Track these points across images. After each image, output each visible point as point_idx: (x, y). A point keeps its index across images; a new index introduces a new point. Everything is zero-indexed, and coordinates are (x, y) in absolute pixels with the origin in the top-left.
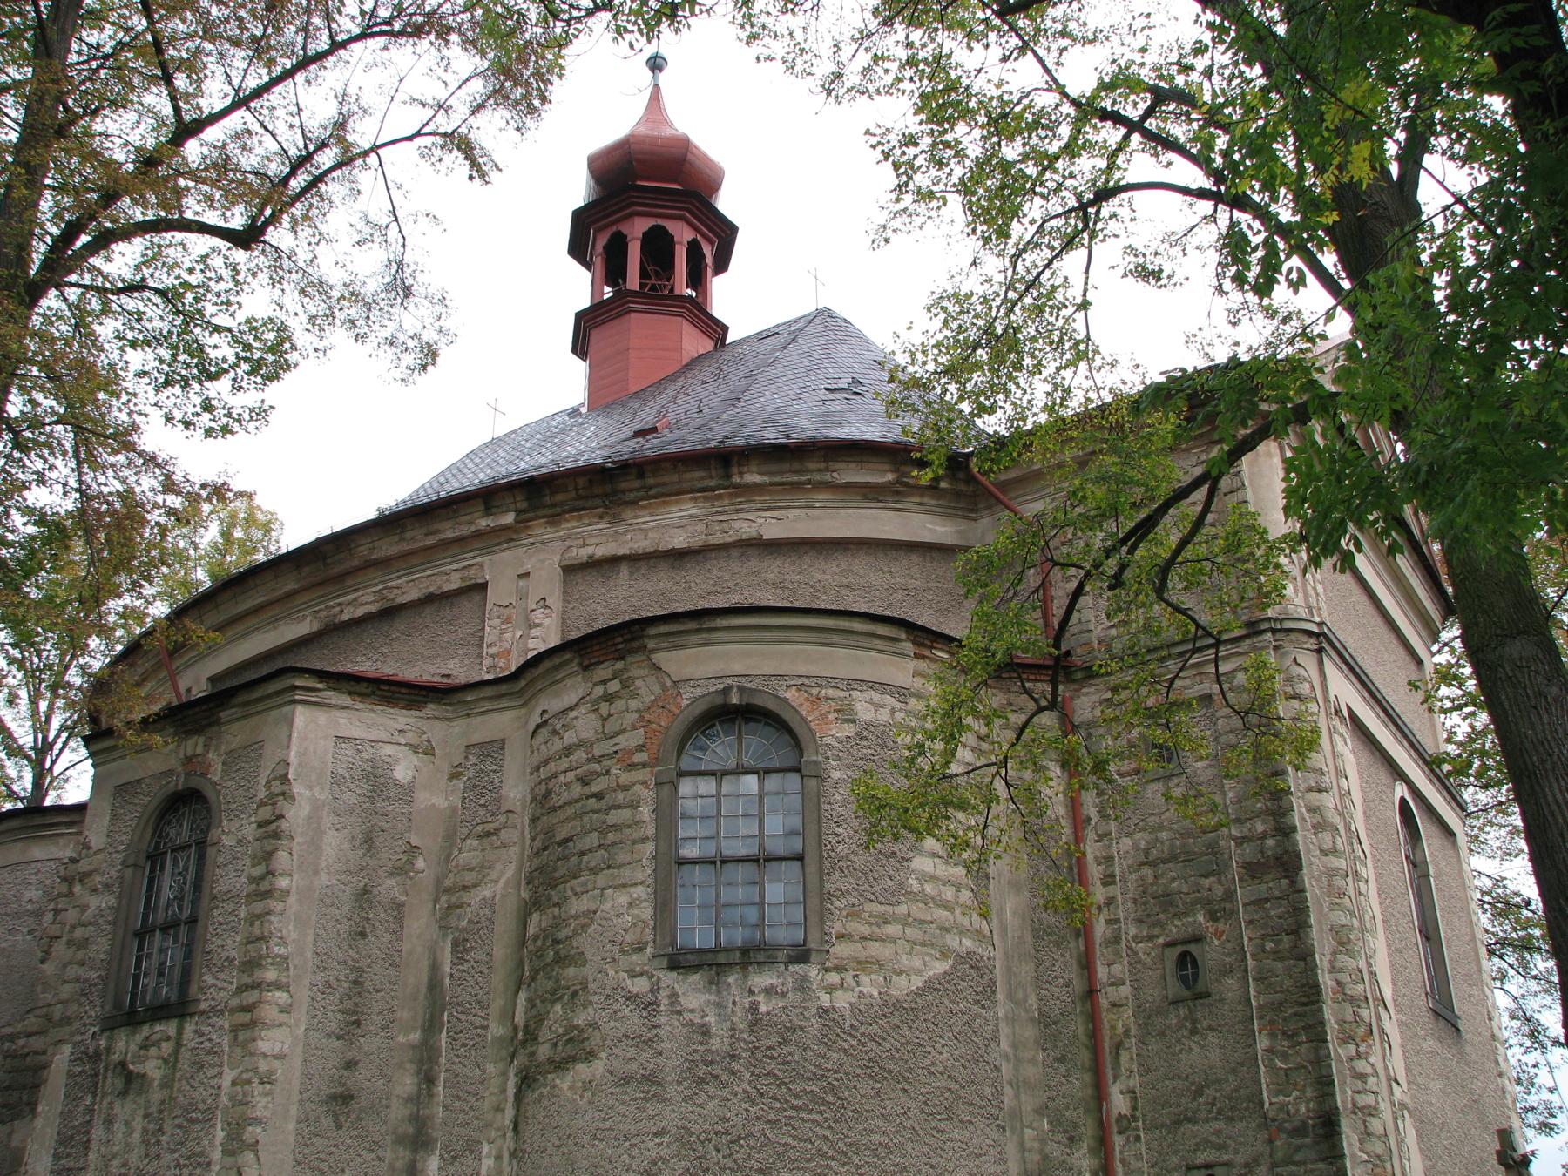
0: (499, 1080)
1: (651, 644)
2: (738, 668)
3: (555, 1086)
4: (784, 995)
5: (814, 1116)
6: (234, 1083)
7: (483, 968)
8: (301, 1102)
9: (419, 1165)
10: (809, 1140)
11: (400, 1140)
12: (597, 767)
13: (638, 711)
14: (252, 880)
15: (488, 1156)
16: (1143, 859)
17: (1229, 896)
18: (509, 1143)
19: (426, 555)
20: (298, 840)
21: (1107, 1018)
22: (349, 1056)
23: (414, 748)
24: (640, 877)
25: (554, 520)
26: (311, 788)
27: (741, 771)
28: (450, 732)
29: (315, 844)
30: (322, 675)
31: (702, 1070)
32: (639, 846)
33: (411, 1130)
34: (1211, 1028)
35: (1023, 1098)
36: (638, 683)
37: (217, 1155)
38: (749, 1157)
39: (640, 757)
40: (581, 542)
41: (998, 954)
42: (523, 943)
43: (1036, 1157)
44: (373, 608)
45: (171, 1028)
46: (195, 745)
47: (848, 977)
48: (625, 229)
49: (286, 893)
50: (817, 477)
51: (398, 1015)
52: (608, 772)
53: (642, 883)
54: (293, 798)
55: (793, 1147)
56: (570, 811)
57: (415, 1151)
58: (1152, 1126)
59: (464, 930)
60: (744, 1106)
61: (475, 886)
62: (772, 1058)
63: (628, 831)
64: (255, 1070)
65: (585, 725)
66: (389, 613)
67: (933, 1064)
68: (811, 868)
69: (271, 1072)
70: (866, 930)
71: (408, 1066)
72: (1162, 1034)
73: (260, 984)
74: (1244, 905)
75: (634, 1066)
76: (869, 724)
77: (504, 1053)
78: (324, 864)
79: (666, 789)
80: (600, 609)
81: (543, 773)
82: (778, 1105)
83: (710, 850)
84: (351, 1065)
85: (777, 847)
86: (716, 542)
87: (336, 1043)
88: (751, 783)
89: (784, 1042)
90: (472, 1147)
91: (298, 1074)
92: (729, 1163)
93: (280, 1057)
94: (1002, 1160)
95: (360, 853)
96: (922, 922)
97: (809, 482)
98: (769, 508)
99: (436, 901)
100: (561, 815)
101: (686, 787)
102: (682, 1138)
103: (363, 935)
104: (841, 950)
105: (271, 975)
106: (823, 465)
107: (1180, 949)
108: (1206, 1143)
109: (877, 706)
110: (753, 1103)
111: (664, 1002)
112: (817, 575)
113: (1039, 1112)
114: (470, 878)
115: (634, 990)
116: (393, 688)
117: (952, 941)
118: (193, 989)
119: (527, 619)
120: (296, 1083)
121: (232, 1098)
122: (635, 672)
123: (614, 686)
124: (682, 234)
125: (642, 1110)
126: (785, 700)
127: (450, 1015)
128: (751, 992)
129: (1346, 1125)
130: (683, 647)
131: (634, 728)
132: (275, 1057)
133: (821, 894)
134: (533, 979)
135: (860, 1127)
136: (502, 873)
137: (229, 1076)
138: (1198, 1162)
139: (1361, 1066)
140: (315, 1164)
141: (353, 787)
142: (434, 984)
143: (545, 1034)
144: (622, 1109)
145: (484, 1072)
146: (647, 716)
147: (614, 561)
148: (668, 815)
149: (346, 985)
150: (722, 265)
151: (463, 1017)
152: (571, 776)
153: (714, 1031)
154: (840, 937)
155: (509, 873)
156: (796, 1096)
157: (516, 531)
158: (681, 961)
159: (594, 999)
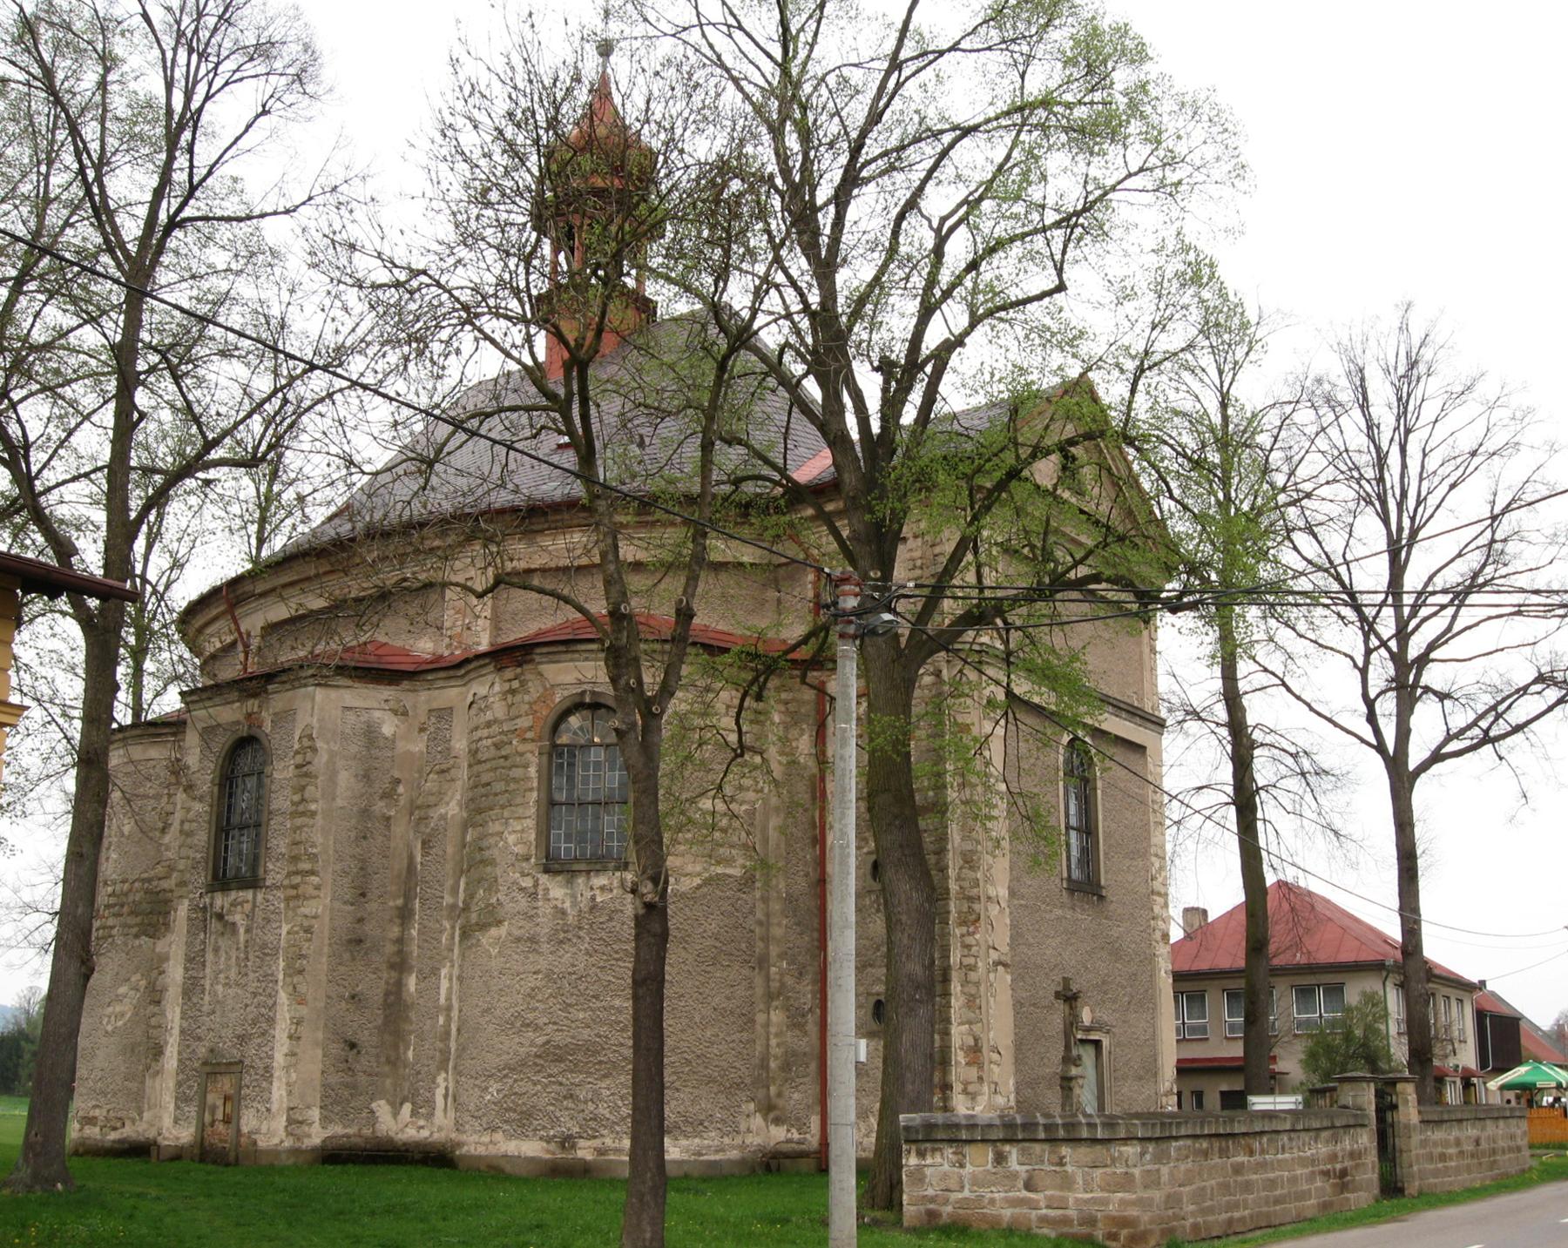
0: (448, 932)
11: (392, 966)
14: (293, 803)
18: (456, 972)
23: (395, 712)
31: (562, 935)
37: (281, 977)
39: (529, 735)
45: (249, 894)
46: (252, 705)
56: (488, 765)
84: (361, 920)
89: (611, 919)
90: (435, 972)
102: (549, 975)
103: (365, 838)
111: (541, 893)
114: (432, 800)
118: (261, 871)
120: (326, 934)
122: (528, 676)
123: (516, 684)
129: (955, 977)
139: (969, 940)
143: (474, 908)
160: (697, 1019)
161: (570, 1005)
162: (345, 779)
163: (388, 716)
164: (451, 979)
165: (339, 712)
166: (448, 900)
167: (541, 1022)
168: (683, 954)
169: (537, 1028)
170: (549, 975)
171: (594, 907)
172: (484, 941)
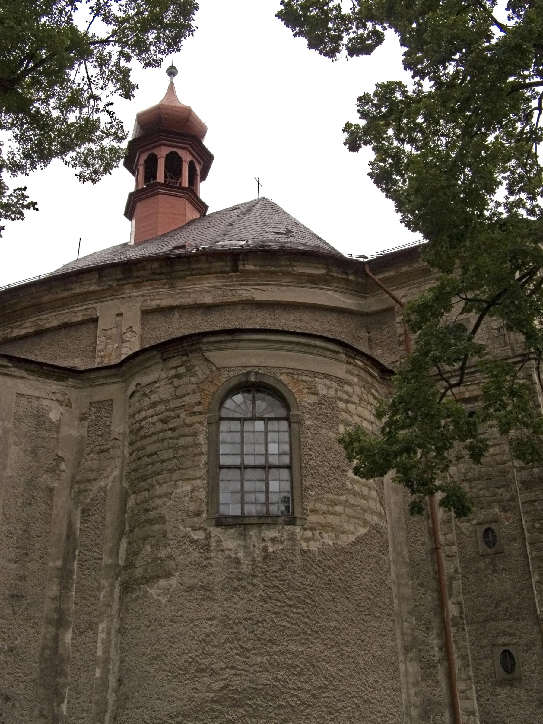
0: (107, 590)
1: (204, 347)
3: (146, 592)
4: (282, 542)
5: (300, 611)
7: (100, 526)
10: (297, 624)
11: (49, 622)
12: (172, 414)
13: (197, 383)
16: (463, 478)
17: (513, 499)
18: (116, 624)
19: (64, 303)
21: (445, 563)
22: (21, 573)
23: (61, 403)
24: (198, 474)
25: (137, 286)
27: (254, 419)
28: (81, 396)
30: (11, 358)
31: (236, 583)
32: (197, 458)
33: (56, 616)
34: (504, 569)
35: (402, 605)
36: (196, 368)
38: (264, 633)
39: (197, 409)
41: (389, 526)
43: (410, 638)
44: (31, 330)
47: (317, 533)
50: (285, 269)
51: (50, 551)
52: (178, 417)
53: (199, 478)
56: (154, 438)
57: (58, 629)
58: (472, 623)
60: (260, 604)
61: (95, 480)
62: (276, 577)
63: (191, 449)
65: (164, 391)
66: (40, 333)
68: (296, 472)
70: (324, 508)
71: (55, 579)
72: (476, 572)
74: (522, 503)
75: (196, 580)
76: (325, 396)
77: (112, 573)
78: (9, 464)
79: (213, 427)
80: (163, 334)
81: (138, 417)
82: (279, 604)
83: (237, 461)
84: (22, 578)
85: (274, 460)
86: (229, 300)
88: (260, 425)
89: (283, 568)
90: (92, 627)
92: (252, 636)
94: (394, 640)
96: (353, 506)
97: (280, 271)
98: (259, 284)
99: (71, 488)
100: (149, 440)
101: (224, 426)
102: (225, 621)
103: (30, 504)
104: (313, 518)
106: (288, 263)
107: (485, 527)
108: (503, 633)
109: (329, 387)
110: (266, 602)
112: (283, 321)
113: (410, 613)
115: (196, 538)
116: (50, 369)
117: (368, 517)
119: (121, 338)
122: (194, 362)
123: (182, 370)
124: (186, 157)
125: (201, 605)
126: (280, 381)
127: (80, 552)
128: (264, 540)
130: (224, 349)
131: (194, 392)
133: (302, 487)
134: (131, 531)
135: (324, 617)
138: (499, 642)
141: (26, 421)
142: (70, 533)
145: (100, 584)
146: (202, 387)
147: (171, 309)
148: (214, 443)
149: (20, 532)
150: (203, 178)
151: (87, 553)
152: (156, 418)
153: (242, 561)
154: (312, 511)
155: (116, 473)
156: (290, 599)
157: (116, 291)
158: (223, 522)
159: (171, 542)
160: (362, 665)
161: (248, 650)
163: (54, 405)
164: (109, 633)
165: (14, 397)
166: (107, 560)
167: (216, 667)
169: (213, 673)
170: (225, 621)
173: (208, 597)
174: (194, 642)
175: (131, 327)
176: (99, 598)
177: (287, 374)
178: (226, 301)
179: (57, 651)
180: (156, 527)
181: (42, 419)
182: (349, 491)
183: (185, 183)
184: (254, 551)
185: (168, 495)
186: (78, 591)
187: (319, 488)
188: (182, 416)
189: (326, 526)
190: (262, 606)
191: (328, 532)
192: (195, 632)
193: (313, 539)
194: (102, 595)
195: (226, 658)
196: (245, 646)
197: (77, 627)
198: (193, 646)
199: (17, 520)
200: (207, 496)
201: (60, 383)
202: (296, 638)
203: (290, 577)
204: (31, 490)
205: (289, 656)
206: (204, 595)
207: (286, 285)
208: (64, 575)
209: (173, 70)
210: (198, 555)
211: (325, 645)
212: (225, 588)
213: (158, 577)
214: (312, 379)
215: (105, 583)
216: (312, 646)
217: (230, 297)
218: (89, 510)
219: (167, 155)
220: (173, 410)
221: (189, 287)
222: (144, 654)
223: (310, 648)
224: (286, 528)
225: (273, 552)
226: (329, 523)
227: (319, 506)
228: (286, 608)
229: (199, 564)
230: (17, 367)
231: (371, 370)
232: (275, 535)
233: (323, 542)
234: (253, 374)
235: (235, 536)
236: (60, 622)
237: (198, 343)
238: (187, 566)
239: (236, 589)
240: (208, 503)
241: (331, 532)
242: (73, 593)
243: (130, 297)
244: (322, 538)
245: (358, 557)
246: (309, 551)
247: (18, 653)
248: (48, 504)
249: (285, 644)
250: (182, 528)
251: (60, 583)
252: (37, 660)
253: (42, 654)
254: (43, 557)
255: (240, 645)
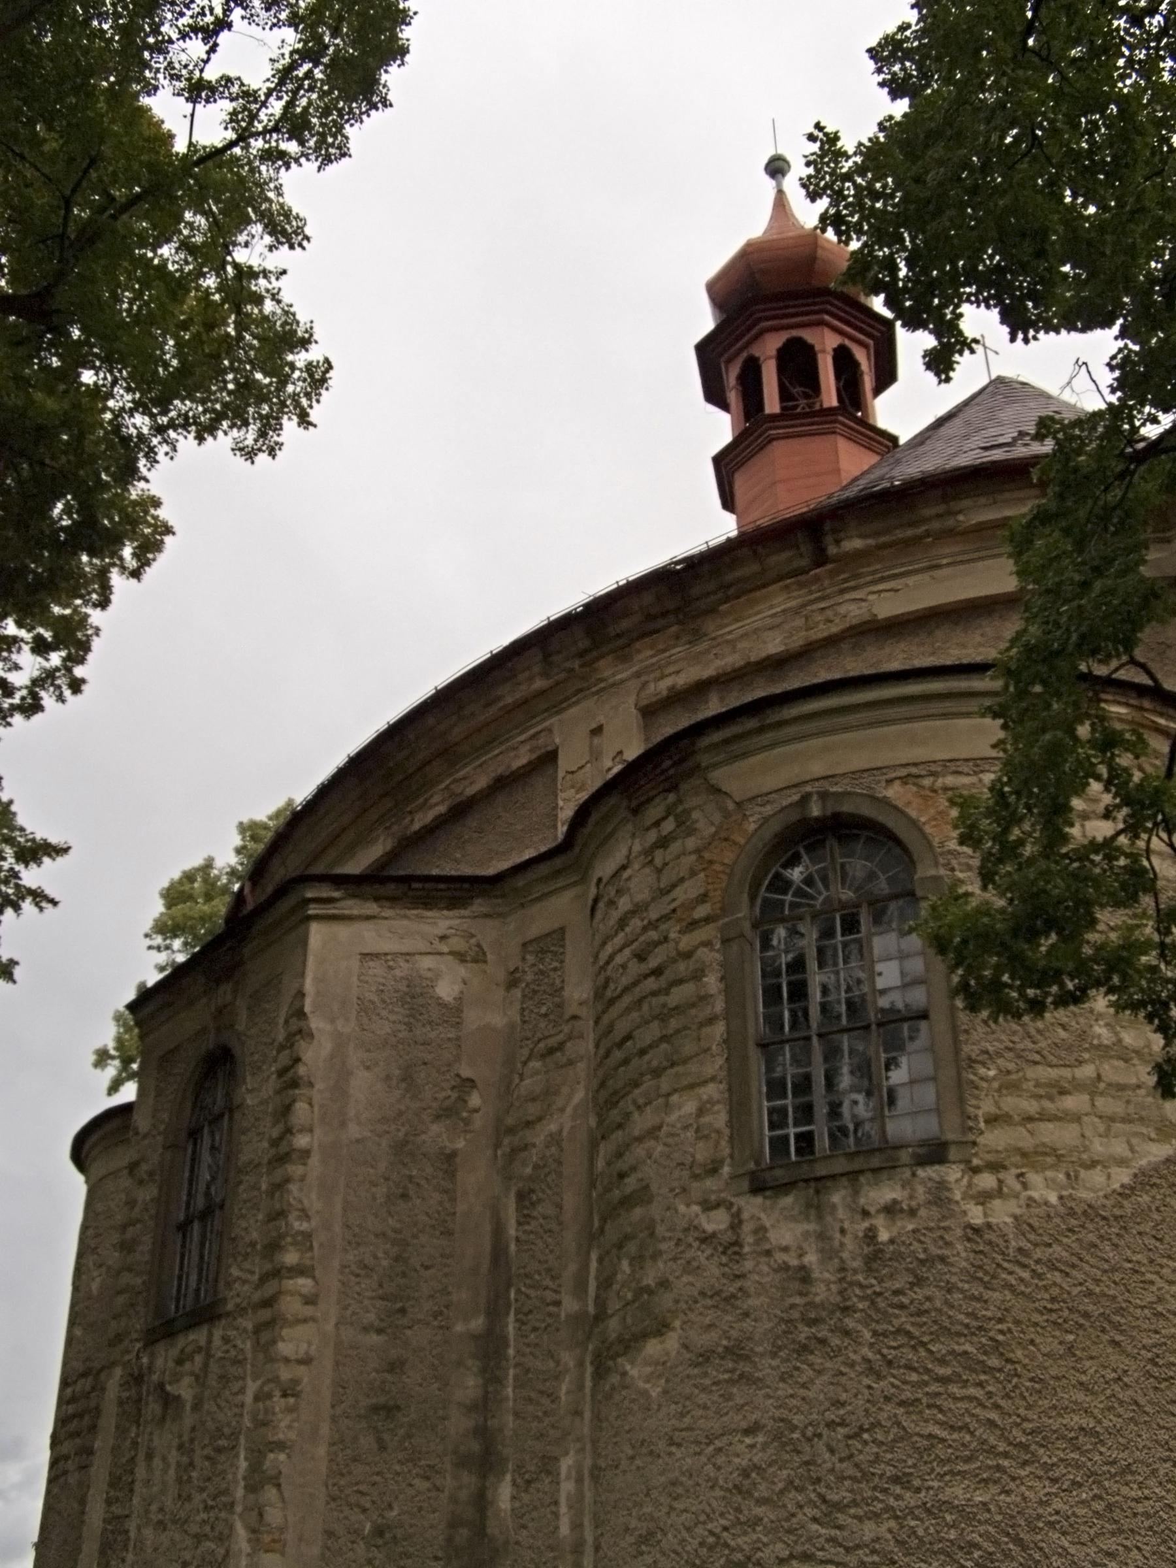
2: (817, 768)
4: (912, 1212)
5: (972, 1391)
6: (257, 1398)
7: (554, 1226)
8: (334, 1419)
9: (489, 1494)
10: (965, 1427)
11: (463, 1462)
15: (568, 1478)
20: (319, 1086)
23: (460, 957)
25: (623, 655)
26: (333, 1021)
29: (340, 1090)
30: (340, 881)
31: (804, 1333)
32: (706, 1030)
36: (695, 815)
37: (240, 1492)
38: (877, 1459)
39: (701, 911)
40: (657, 674)
42: (593, 1185)
44: (442, 809)
45: (198, 1336)
47: (1009, 1177)
48: (756, 351)
49: (306, 1153)
50: (936, 525)
53: (713, 1079)
54: (311, 1036)
55: (943, 1440)
56: (627, 1000)
57: (484, 1477)
59: (530, 1178)
61: (540, 1119)
62: (902, 1307)
63: (693, 1012)
64: (276, 1379)
66: (460, 811)
67: (1160, 1300)
69: (296, 1382)
70: (1031, 1107)
71: (470, 1362)
73: (279, 1271)
75: (714, 1335)
82: (914, 1377)
84: (395, 1367)
86: (820, 635)
87: (375, 1338)
89: (919, 1282)
90: (548, 1465)
91: (328, 1381)
93: (306, 1361)
95: (398, 1093)
96: (1121, 1087)
97: (928, 534)
98: (882, 580)
99: (497, 1145)
103: (405, 1196)
104: (994, 1139)
105: (291, 1258)
106: (941, 509)
110: (879, 1377)
114: (533, 1110)
115: (710, 1228)
120: (327, 1394)
121: (254, 1419)
122: (691, 802)
123: (669, 826)
124: (826, 342)
125: (728, 1397)
126: (885, 802)
127: (518, 1291)
128: (866, 1214)
130: (745, 755)
131: (693, 873)
132: (300, 1362)
133: (957, 1061)
136: (570, 1097)
137: (252, 1387)
140: (353, 1499)
142: (498, 1254)
144: (703, 1398)
145: (558, 1363)
146: (707, 855)
149: (385, 1263)
152: (627, 952)
153: (816, 1274)
154: (992, 1120)
155: (580, 1095)
156: (942, 1362)
159: (663, 1246)
161: (839, 1507)
162: (362, 1084)
164: (579, 1480)
165: (355, 963)
166: (570, 1305)
168: (1115, 1358)
171: (875, 1256)
172: (634, 1372)
173: (741, 1376)
174: (718, 1493)
175: (620, 753)
176: (558, 1398)
177: (904, 780)
178: (814, 637)
179: (484, 1527)
180: (638, 1212)
181: (420, 1001)
182: (1103, 1051)
183: (830, 397)
184: (842, 1245)
185: (653, 1132)
186: (519, 1384)
187: (1010, 1055)
188: (672, 935)
189: (1036, 1153)
190: (869, 1387)
191: (1039, 1168)
192: (719, 1468)
193: (999, 1192)
194: (564, 1388)
195: (789, 1531)
196: (833, 1497)
197: (519, 1468)
198: (714, 1503)
199: (376, 1236)
200: (730, 1124)
201: (456, 912)
202: (966, 1467)
203: (938, 1304)
204: (405, 1165)
205: (948, 1518)
206: (732, 1371)
207: (948, 565)
208: (490, 1348)
209: (781, 163)
210: (717, 1272)
211: (1054, 1481)
212: (780, 1348)
213: (645, 1336)
214: (974, 779)
215: (568, 1358)
216: (1012, 1485)
217: (822, 626)
218: (532, 1191)
219: (779, 351)
220: (653, 925)
221: (734, 628)
222: (627, 1529)
223: (1008, 1493)
224: (921, 1173)
225: (892, 1241)
226: (1044, 1145)
227: (1012, 1103)
228: (934, 1388)
229: (718, 1293)
230: (354, 896)
231: (1162, 721)
232: (894, 1195)
233: (1030, 1198)
234: (815, 797)
235: (795, 1212)
236: (485, 1461)
237: (693, 753)
238: (696, 1302)
239: (804, 1349)
240: (731, 1137)
241: (1052, 1167)
242: (510, 1390)
243: (613, 685)
244: (1025, 1186)
245: (1147, 1227)
246: (989, 1226)
247: (395, 1537)
248: (446, 1191)
249: (936, 1484)
250: (682, 1208)
251: (483, 1370)
252: (440, 1554)
253: (449, 1540)
254: (441, 1313)
255: (820, 1495)
